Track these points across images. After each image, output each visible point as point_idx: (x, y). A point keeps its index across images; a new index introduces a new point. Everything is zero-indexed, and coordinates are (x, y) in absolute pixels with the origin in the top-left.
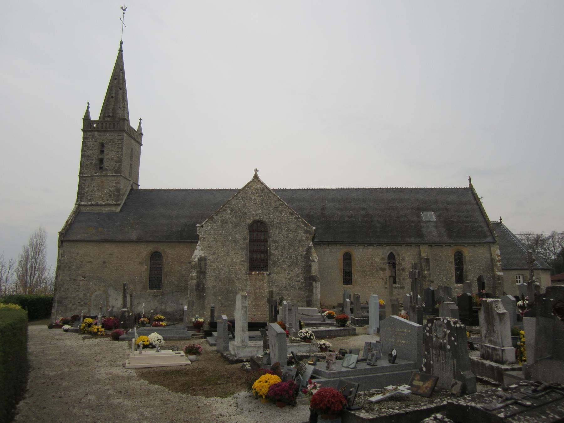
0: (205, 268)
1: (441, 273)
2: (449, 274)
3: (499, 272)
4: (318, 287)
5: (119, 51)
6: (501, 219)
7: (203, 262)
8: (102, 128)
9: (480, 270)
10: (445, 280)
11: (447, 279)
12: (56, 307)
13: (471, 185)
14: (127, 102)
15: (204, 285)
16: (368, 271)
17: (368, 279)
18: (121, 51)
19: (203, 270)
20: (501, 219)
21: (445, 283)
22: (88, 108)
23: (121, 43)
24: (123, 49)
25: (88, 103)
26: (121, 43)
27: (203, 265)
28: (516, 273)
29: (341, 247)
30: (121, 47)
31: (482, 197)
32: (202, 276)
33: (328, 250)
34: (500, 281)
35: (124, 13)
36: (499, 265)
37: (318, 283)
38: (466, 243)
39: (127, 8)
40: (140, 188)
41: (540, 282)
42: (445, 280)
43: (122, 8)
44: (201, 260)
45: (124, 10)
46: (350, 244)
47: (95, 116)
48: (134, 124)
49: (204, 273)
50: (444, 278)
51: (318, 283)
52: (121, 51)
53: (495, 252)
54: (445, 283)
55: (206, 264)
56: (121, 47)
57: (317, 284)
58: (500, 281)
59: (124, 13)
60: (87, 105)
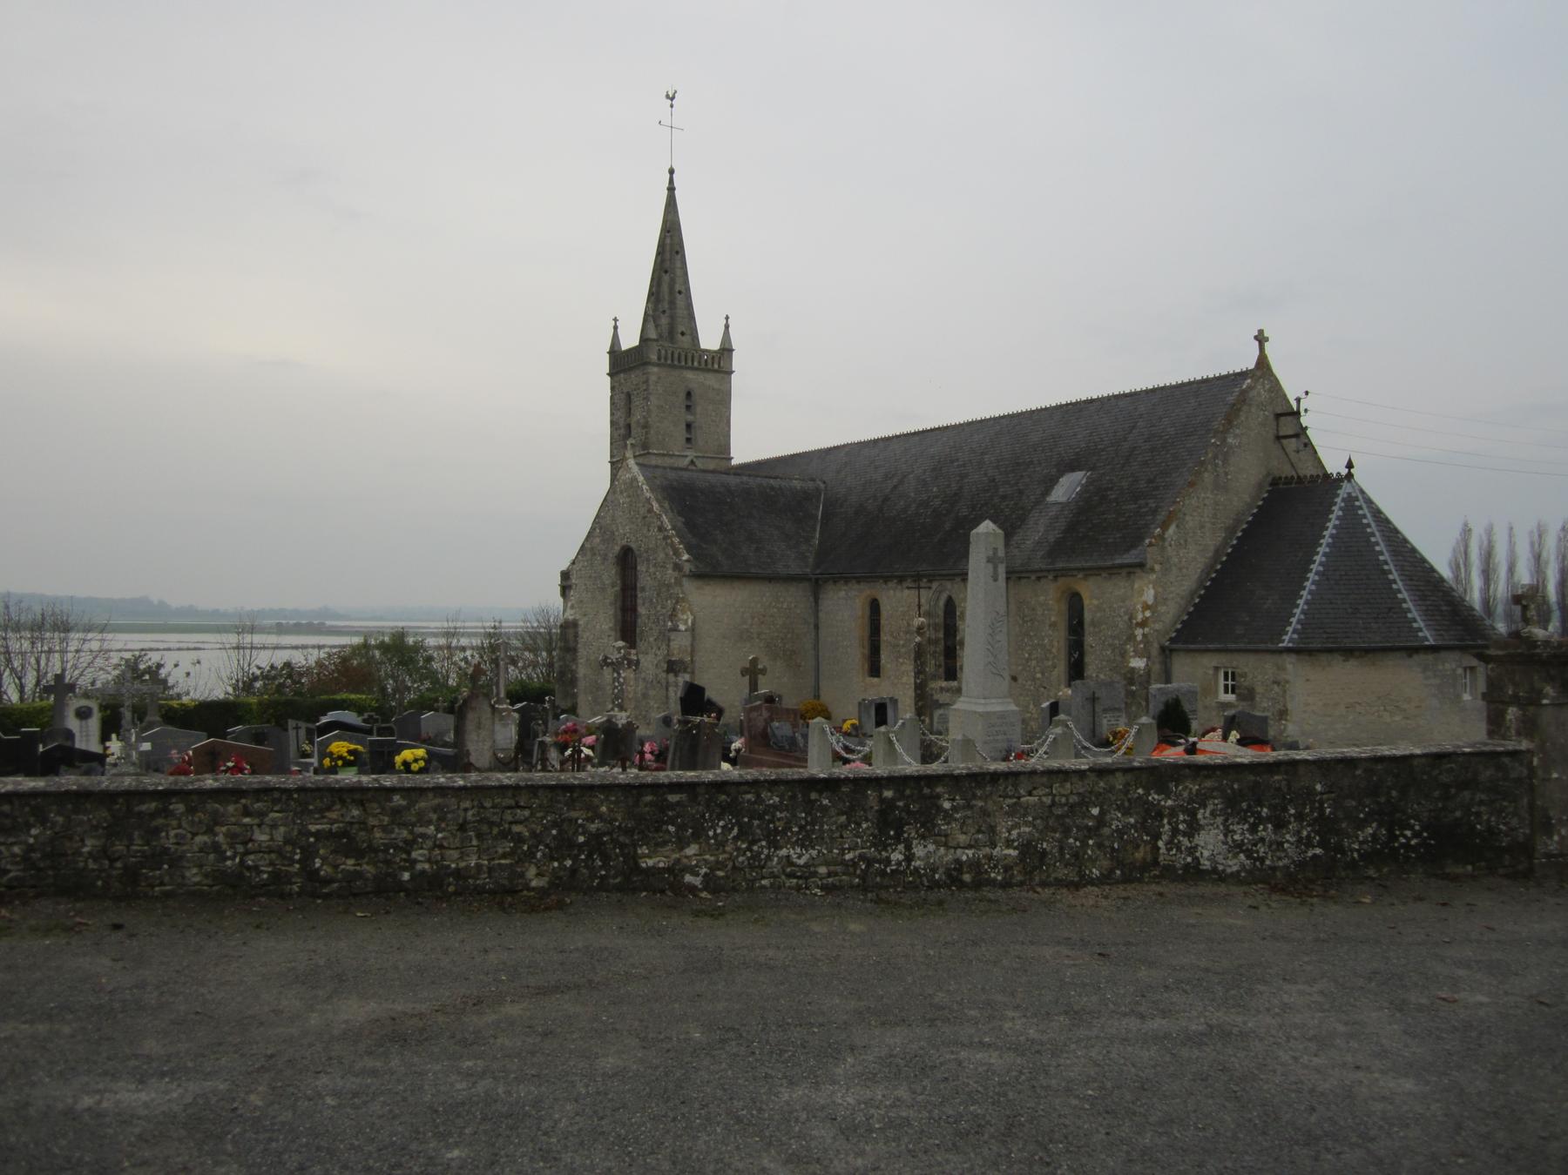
1: (1033, 657)
2: (1048, 660)
3: (1137, 659)
5: (669, 189)
6: (1350, 465)
7: (571, 631)
8: (659, 359)
9: (1113, 651)
10: (1039, 675)
11: (1043, 674)
13: (1262, 362)
14: (689, 297)
15: (573, 673)
16: (903, 646)
17: (902, 664)
18: (671, 189)
19: (572, 644)
20: (1350, 465)
21: (1038, 682)
23: (671, 172)
25: (616, 320)
26: (671, 172)
27: (571, 637)
28: (1214, 663)
29: (862, 586)
30: (671, 181)
31: (1307, 393)
32: (568, 657)
33: (842, 594)
34: (1134, 688)
35: (672, 106)
36: (1139, 638)
38: (1079, 570)
39: (676, 92)
40: (734, 462)
42: (1039, 675)
43: (667, 96)
44: (565, 628)
45: (672, 99)
47: (630, 340)
48: (709, 340)
49: (574, 650)
50: (1038, 669)
53: (1141, 595)
54: (1038, 682)
55: (576, 635)
56: (671, 181)
58: (1134, 688)
59: (672, 106)
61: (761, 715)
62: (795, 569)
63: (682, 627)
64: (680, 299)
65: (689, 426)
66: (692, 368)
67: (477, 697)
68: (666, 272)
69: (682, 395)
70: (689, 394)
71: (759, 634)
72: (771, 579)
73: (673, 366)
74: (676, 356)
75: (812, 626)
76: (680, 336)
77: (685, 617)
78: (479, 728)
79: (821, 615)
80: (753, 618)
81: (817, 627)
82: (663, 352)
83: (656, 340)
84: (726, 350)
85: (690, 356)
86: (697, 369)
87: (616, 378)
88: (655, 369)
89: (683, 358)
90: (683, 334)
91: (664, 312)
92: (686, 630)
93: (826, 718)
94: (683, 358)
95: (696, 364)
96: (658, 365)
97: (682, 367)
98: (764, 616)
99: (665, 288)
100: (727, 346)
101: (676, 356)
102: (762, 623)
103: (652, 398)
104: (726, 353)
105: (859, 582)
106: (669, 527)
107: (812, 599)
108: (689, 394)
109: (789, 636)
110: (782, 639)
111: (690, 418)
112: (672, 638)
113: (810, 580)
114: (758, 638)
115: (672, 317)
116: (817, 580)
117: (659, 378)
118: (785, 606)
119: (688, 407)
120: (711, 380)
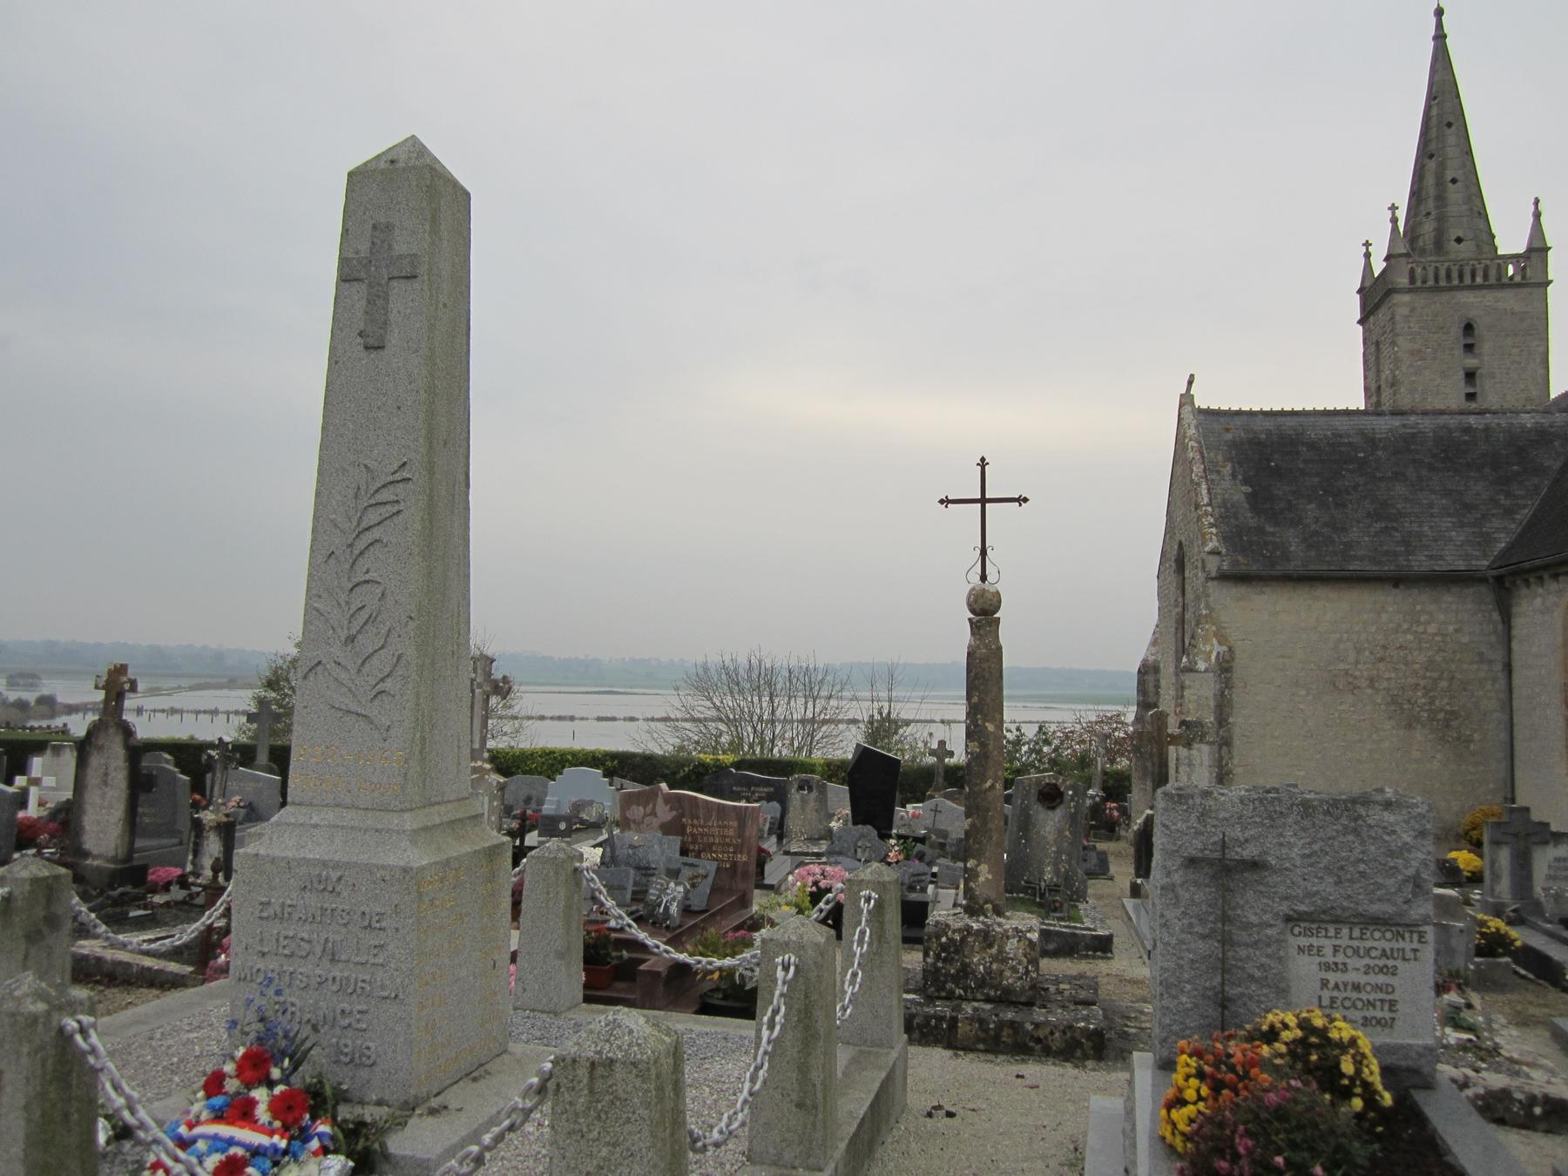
0: (1157, 693)
4: (1197, 762)
7: (1150, 678)
8: (1412, 279)
12: (358, 1110)
18: (1440, 37)
19: (1151, 699)
22: (1537, 215)
24: (1446, 30)
26: (1439, 13)
27: (1151, 687)
30: (1439, 25)
37: (1199, 750)
41: (900, 999)
44: (1146, 673)
46: (1179, 635)
48: (1510, 239)
51: (1199, 750)
52: (1440, 37)
56: (1439, 25)
57: (1194, 752)
60: (1532, 208)
61: (654, 814)
62: (1453, 561)
63: (1202, 666)
64: (1454, 194)
65: (1470, 376)
66: (1473, 287)
67: (107, 728)
68: (1431, 156)
69: (1456, 330)
70: (1469, 328)
71: (1372, 681)
72: (1399, 581)
73: (1437, 289)
74: (1443, 273)
75: (1498, 667)
76: (1453, 244)
77: (1208, 648)
78: (105, 783)
79: (1515, 645)
80: (1359, 651)
81: (1508, 668)
82: (1419, 271)
83: (1407, 255)
84: (1538, 250)
85: (1467, 270)
86: (1480, 287)
87: (1367, 325)
88: (1406, 298)
89: (1455, 275)
90: (1459, 240)
91: (1428, 214)
92: (1206, 671)
93: (1478, 856)
94: (1455, 275)
95: (1479, 280)
96: (1409, 291)
97: (1451, 289)
98: (1384, 647)
99: (1430, 180)
100: (1536, 245)
101: (1443, 273)
102: (1382, 659)
103: (1400, 340)
104: (1535, 256)
105: (1555, 576)
106: (1206, 500)
107: (1496, 616)
108: (1469, 328)
109: (1444, 684)
110: (1427, 691)
111: (1471, 362)
112: (1187, 683)
113: (1483, 580)
114: (1371, 686)
115: (1441, 219)
116: (1499, 579)
117: (1413, 310)
118: (1432, 629)
119: (1469, 348)
120: (1508, 300)
